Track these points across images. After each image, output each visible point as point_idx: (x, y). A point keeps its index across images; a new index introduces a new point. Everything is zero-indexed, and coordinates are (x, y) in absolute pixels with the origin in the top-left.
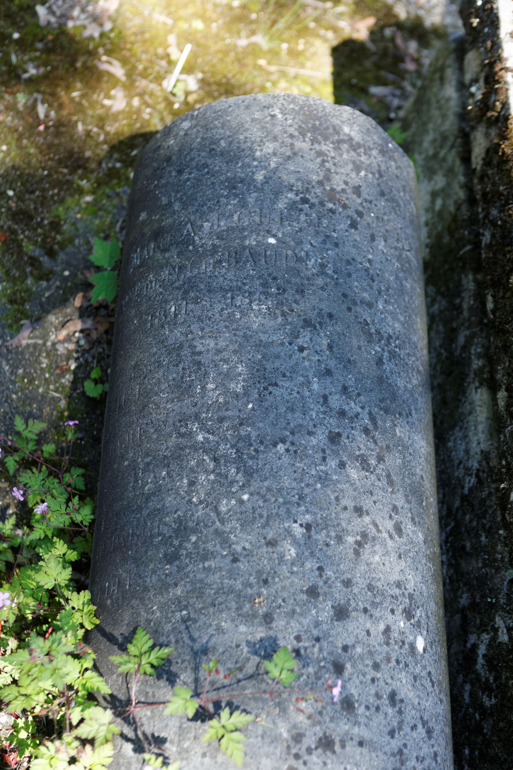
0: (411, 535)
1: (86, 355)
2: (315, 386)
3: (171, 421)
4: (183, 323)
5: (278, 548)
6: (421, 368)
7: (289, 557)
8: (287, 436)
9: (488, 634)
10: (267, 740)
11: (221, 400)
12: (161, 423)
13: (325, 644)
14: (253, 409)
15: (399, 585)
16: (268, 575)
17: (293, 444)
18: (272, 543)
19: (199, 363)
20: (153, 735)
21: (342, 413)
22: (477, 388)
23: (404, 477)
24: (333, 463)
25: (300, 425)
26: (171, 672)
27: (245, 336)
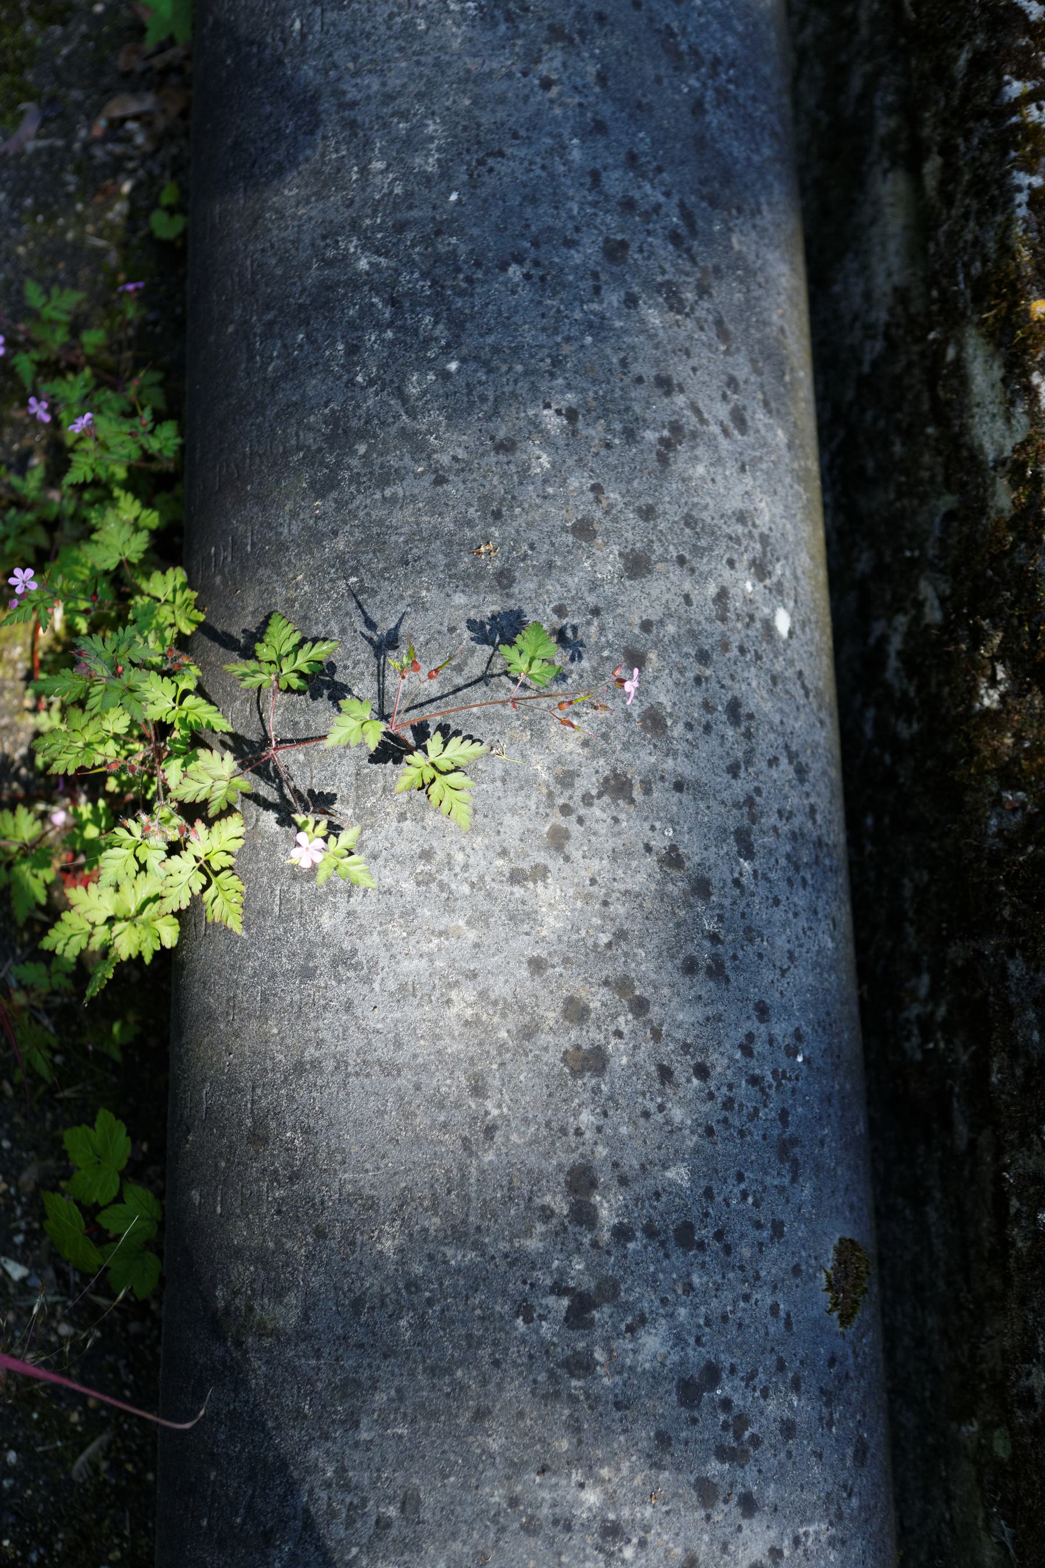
0: (763, 431)
1: (149, 163)
2: (576, 155)
3: (307, 239)
4: (317, 50)
5: (518, 454)
6: (778, 128)
7: (539, 470)
8: (526, 250)
9: (906, 613)
10: (512, 785)
11: (398, 190)
12: (289, 245)
13: (608, 619)
14: (459, 202)
15: (741, 517)
16: (500, 504)
17: (537, 263)
18: (506, 447)
19: (353, 125)
20: (311, 792)
21: (628, 205)
22: (885, 172)
23: (748, 327)
24: (613, 298)
25: (550, 229)
26: (336, 683)
27: (437, 64)
